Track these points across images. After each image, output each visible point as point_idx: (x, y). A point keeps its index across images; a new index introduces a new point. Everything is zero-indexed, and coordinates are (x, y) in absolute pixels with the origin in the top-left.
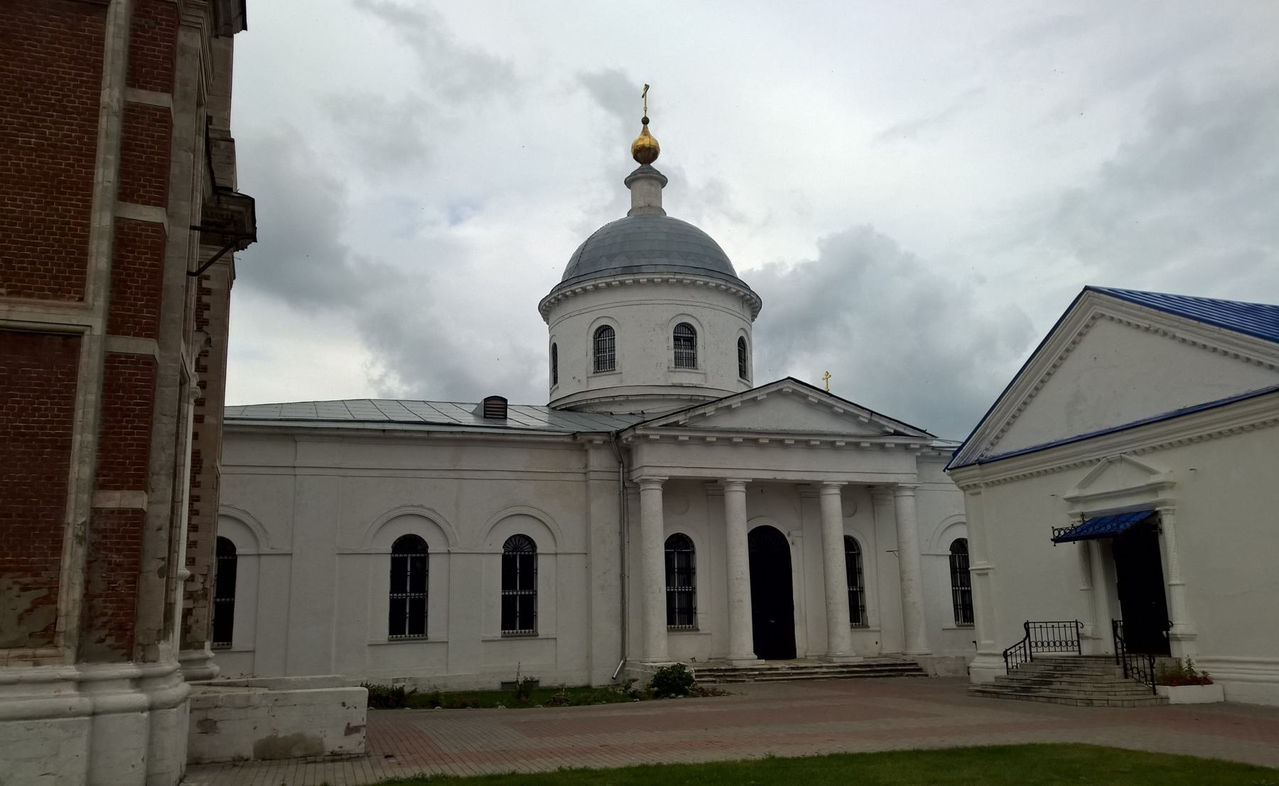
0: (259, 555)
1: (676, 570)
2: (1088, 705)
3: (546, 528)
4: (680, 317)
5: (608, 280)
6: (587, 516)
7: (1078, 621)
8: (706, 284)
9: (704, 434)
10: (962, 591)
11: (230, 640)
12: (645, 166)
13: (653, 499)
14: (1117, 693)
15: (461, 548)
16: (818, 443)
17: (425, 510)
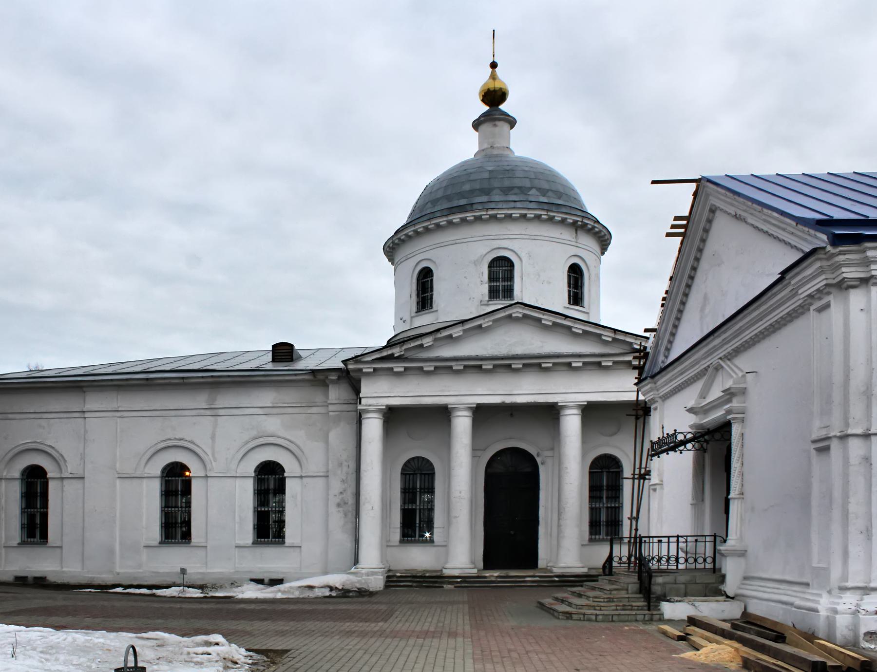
0: (62, 479)
1: (39, 494)
2: (568, 618)
3: (288, 453)
4: (495, 251)
5: (425, 224)
6: (327, 442)
7: (716, 535)
9: (418, 343)
10: (40, 512)
11: (284, 537)
12: (494, 108)
13: (373, 427)
14: (602, 608)
15: (216, 473)
16: (550, 365)
17: (186, 443)
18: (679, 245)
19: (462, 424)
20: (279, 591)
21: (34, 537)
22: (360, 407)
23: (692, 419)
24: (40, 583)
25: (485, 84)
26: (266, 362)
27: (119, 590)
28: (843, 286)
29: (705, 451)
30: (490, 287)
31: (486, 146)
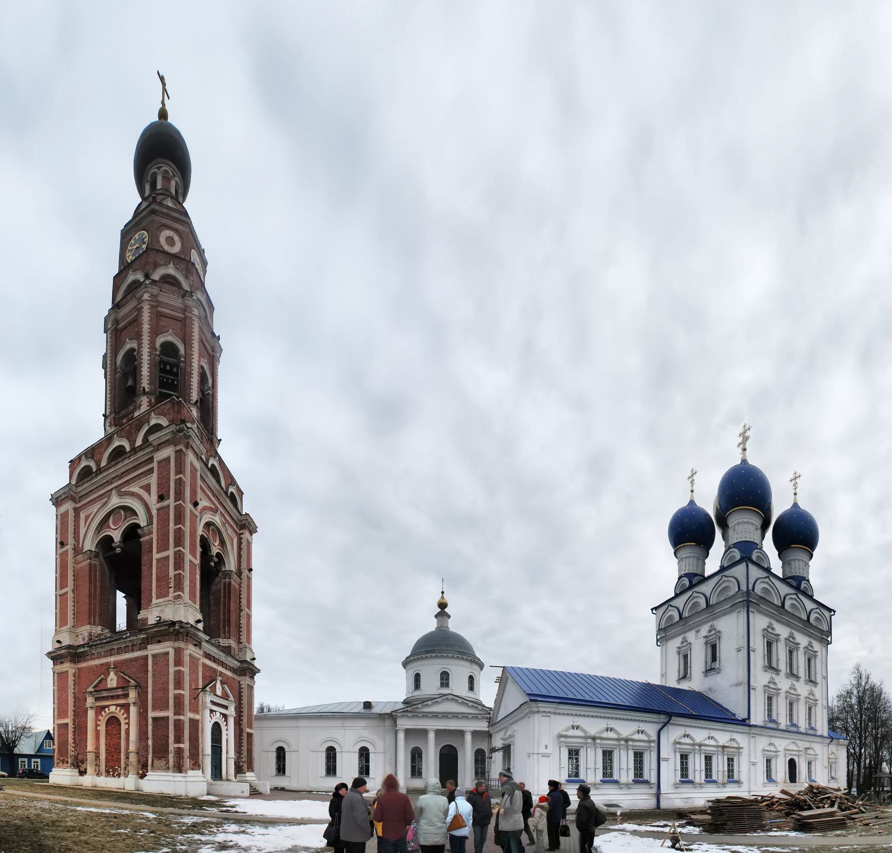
0: (290, 751)
8: (453, 656)
9: (417, 714)
11: (369, 775)
13: (401, 736)
18: (498, 685)
19: (432, 736)
20: (371, 794)
21: (280, 773)
22: (397, 728)
23: (502, 742)
24: (283, 789)
25: (439, 600)
26: (360, 708)
27: (315, 792)
28: (533, 712)
29: (505, 752)
30: (441, 682)
31: (439, 626)
